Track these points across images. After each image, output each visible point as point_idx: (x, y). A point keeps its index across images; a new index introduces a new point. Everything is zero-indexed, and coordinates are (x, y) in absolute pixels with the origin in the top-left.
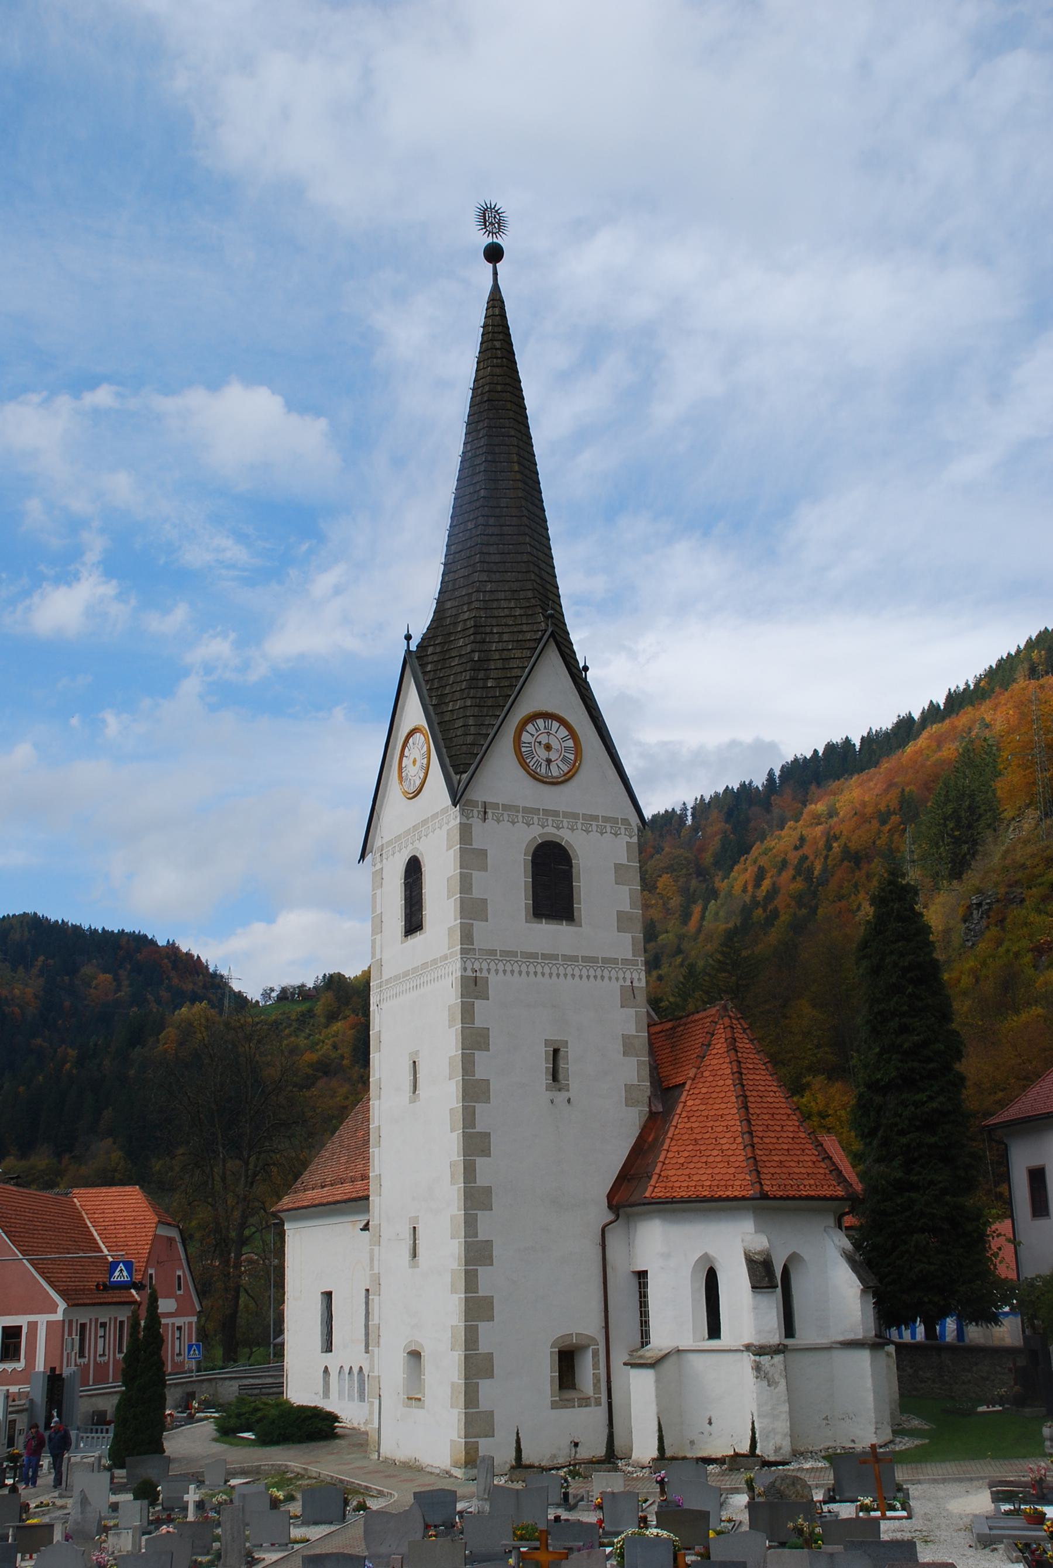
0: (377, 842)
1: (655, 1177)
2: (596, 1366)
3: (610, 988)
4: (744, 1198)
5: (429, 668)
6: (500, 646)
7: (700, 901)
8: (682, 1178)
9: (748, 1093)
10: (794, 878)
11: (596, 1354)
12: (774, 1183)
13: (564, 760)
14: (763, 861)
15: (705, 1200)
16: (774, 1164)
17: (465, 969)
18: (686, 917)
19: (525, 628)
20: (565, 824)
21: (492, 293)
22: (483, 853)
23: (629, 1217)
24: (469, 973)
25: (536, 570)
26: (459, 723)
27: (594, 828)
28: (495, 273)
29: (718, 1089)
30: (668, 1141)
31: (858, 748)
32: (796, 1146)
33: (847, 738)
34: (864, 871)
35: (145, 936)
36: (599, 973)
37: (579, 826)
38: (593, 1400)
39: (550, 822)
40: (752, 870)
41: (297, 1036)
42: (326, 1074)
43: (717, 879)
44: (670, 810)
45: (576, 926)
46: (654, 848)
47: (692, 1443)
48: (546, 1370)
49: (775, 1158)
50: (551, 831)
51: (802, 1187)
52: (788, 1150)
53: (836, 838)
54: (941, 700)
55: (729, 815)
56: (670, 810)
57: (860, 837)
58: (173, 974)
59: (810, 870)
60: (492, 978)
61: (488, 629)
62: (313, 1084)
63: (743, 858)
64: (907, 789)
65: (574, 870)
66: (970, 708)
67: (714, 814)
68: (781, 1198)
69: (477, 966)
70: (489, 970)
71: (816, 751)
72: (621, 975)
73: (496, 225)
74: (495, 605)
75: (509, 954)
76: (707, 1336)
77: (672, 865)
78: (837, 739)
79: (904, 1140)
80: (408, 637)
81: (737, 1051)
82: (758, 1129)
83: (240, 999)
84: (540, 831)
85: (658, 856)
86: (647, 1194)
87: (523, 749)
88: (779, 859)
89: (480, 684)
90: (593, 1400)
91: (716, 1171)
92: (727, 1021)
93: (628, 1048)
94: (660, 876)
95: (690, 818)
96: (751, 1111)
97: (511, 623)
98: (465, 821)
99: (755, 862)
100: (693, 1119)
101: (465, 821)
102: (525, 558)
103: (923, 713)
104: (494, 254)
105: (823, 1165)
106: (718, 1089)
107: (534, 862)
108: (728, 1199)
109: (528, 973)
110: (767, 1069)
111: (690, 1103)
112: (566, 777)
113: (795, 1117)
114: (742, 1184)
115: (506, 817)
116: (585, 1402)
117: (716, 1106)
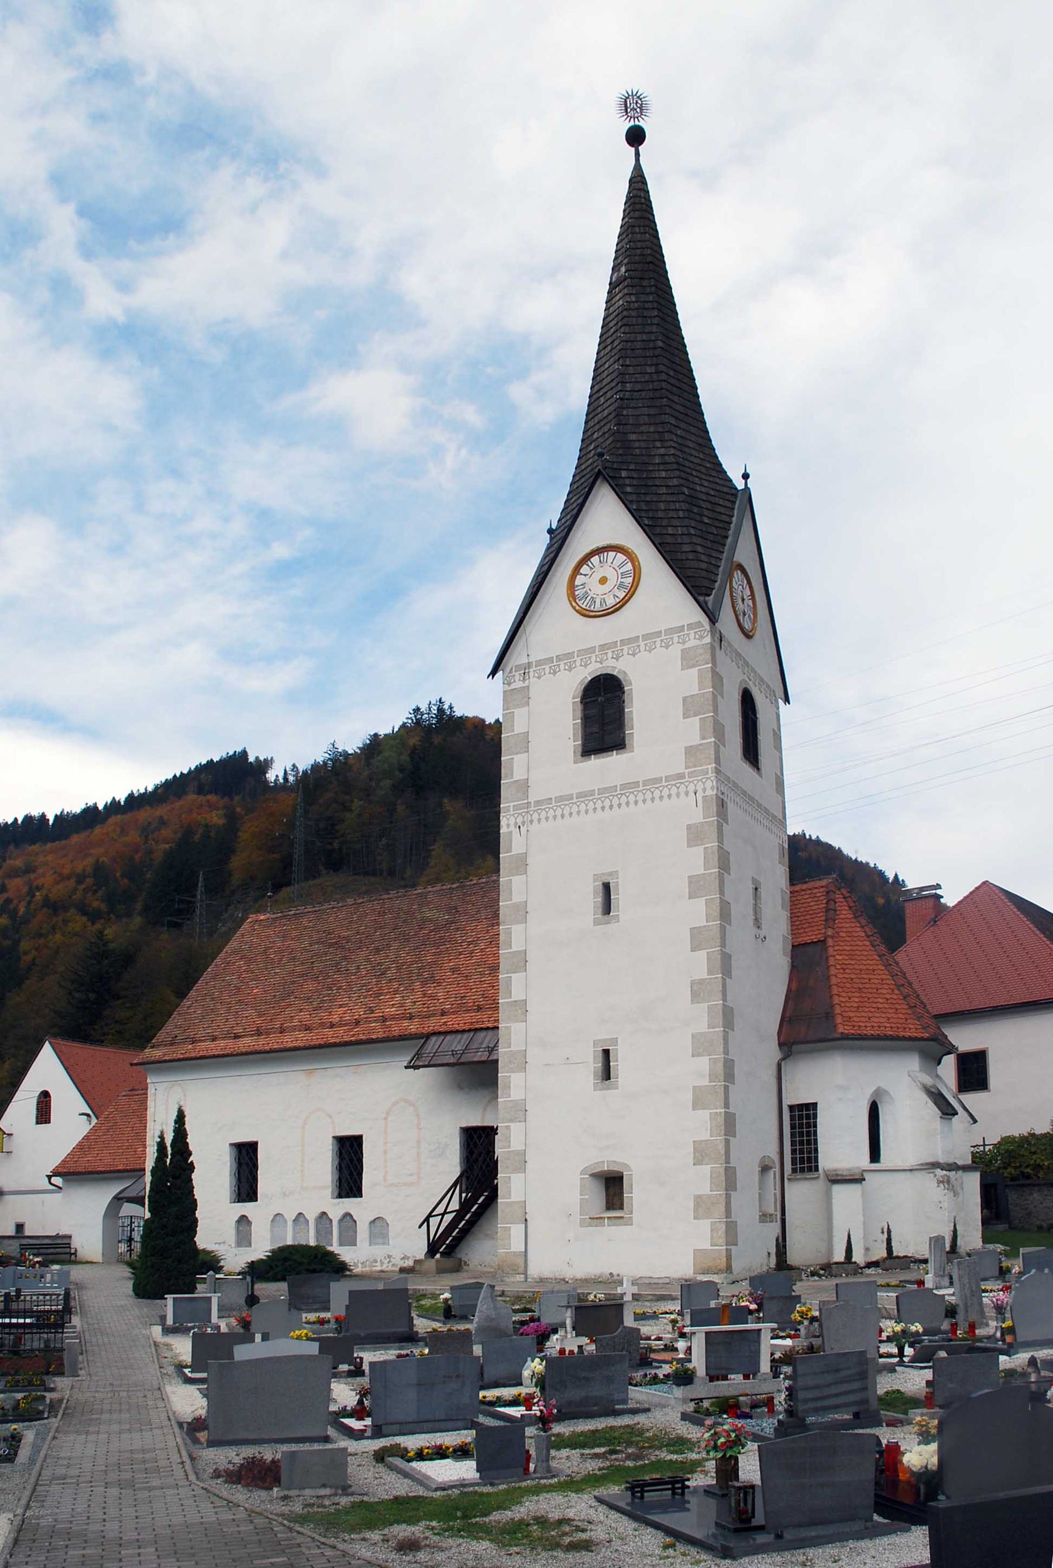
0: (517, 657)
21: (635, 168)
28: (637, 154)
31: (51, 822)
33: (43, 813)
52: (858, 1007)
53: (38, 888)
56: (59, 814)
59: (16, 910)
64: (101, 860)
66: (148, 808)
71: (16, 819)
73: (638, 110)
78: (36, 813)
103: (106, 805)
104: (635, 137)
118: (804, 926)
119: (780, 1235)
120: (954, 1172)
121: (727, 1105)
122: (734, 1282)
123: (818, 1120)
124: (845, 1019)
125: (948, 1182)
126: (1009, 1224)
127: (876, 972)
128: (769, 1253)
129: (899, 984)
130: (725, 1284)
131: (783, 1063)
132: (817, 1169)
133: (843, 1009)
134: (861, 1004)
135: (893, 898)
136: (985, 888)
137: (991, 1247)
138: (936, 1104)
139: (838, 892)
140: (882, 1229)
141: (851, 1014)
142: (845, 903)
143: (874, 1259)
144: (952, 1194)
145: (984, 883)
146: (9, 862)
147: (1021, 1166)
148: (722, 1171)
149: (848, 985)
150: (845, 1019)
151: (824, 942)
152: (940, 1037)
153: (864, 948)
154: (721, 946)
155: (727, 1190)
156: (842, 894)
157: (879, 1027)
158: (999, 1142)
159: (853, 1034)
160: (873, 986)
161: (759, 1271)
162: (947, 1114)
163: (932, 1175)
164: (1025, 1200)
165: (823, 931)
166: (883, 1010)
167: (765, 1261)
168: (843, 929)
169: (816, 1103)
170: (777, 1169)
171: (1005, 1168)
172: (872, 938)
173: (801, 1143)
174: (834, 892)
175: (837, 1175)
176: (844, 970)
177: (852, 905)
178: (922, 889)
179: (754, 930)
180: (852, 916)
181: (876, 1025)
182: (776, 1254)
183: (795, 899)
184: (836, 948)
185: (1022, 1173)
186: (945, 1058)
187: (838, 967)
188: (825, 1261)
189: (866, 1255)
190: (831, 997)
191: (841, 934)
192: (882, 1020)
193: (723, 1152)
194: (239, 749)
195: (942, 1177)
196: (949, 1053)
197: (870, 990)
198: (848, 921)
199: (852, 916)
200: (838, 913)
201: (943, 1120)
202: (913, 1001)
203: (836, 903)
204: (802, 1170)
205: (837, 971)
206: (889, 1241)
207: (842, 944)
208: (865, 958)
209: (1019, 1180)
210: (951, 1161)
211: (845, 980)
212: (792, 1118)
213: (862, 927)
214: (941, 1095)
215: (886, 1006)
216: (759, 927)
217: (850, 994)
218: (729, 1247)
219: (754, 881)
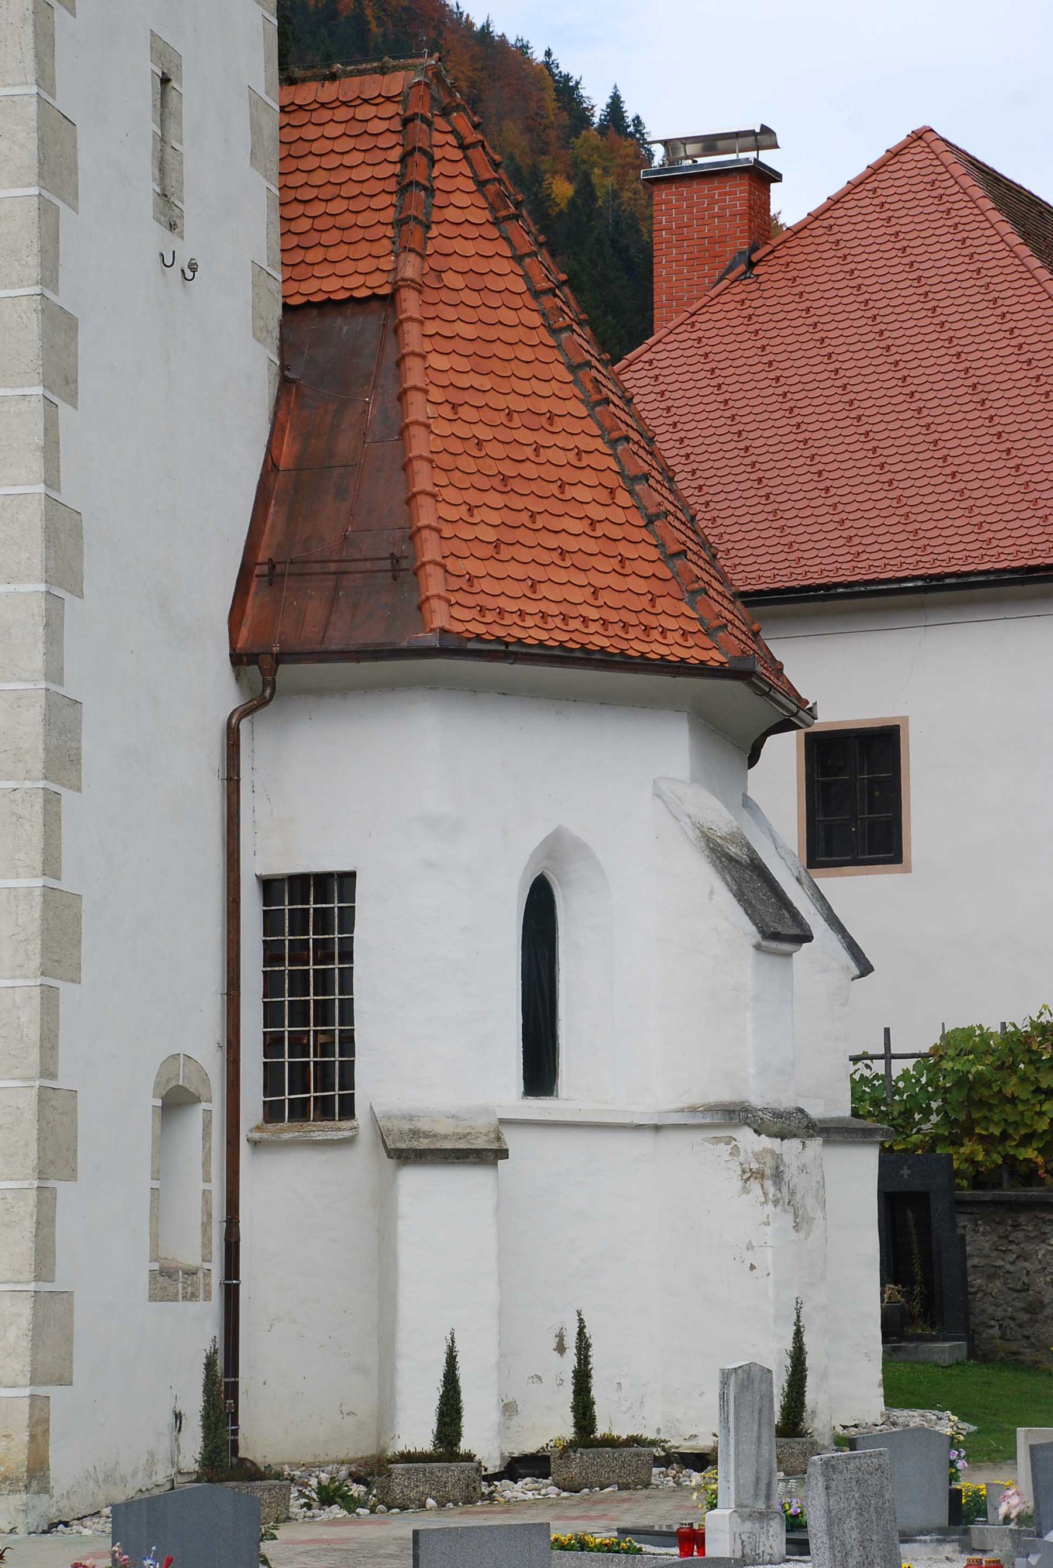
52: (497, 545)
118: (326, 239)
119: (220, 1345)
120: (794, 1144)
121: (51, 865)
122: (52, 1527)
123: (356, 935)
124: (456, 583)
125: (778, 1176)
126: (970, 1341)
127: (559, 424)
128: (178, 1417)
129: (631, 471)
130: (22, 1531)
131: (244, 725)
132: (348, 1110)
133: (448, 548)
134: (509, 536)
135: (603, 183)
136: (918, 153)
137: (913, 1418)
138: (741, 896)
139: (440, 123)
140: (561, 1337)
141: (475, 567)
142: (464, 168)
143: (531, 1446)
144: (789, 1219)
145: (921, 136)
147: (1005, 1136)
148: (28, 1102)
149: (467, 464)
150: (456, 583)
151: (390, 300)
152: (759, 669)
153: (520, 333)
154: (42, 282)
155: (42, 1175)
156: (454, 132)
157: (565, 618)
158: (936, 1048)
159: (478, 637)
160: (553, 473)
161: (141, 1482)
162: (776, 937)
163: (724, 1149)
164: (1023, 1256)
165: (387, 264)
166: (580, 560)
167: (164, 1447)
168: (455, 262)
169: (352, 875)
170: (216, 1104)
171: (955, 1141)
172: (548, 302)
173: (299, 1014)
174: (429, 123)
175: (415, 1133)
176: (454, 407)
177: (487, 173)
178: (710, 143)
179: (155, 236)
180: (487, 215)
181: (553, 609)
182: (206, 1417)
183: (295, 134)
184: (431, 328)
185: (1010, 1161)
186: (772, 741)
187: (436, 395)
188: (363, 1448)
189: (504, 1428)
190: (410, 500)
191: (449, 279)
192: (577, 596)
193: (33, 1033)
195: (757, 1156)
196: (784, 726)
197: (537, 487)
198: (474, 232)
199: (487, 215)
200: (439, 199)
201: (762, 957)
202: (675, 536)
203: (433, 162)
204: (299, 1111)
205: (430, 410)
206: (582, 1378)
207: (450, 314)
208: (525, 371)
209: (998, 1185)
210: (787, 1102)
211: (457, 447)
212: (271, 922)
213: (518, 259)
214: (758, 869)
215: (591, 546)
216: (172, 227)
217: (473, 498)
218: (42, 1391)
219: (160, 49)
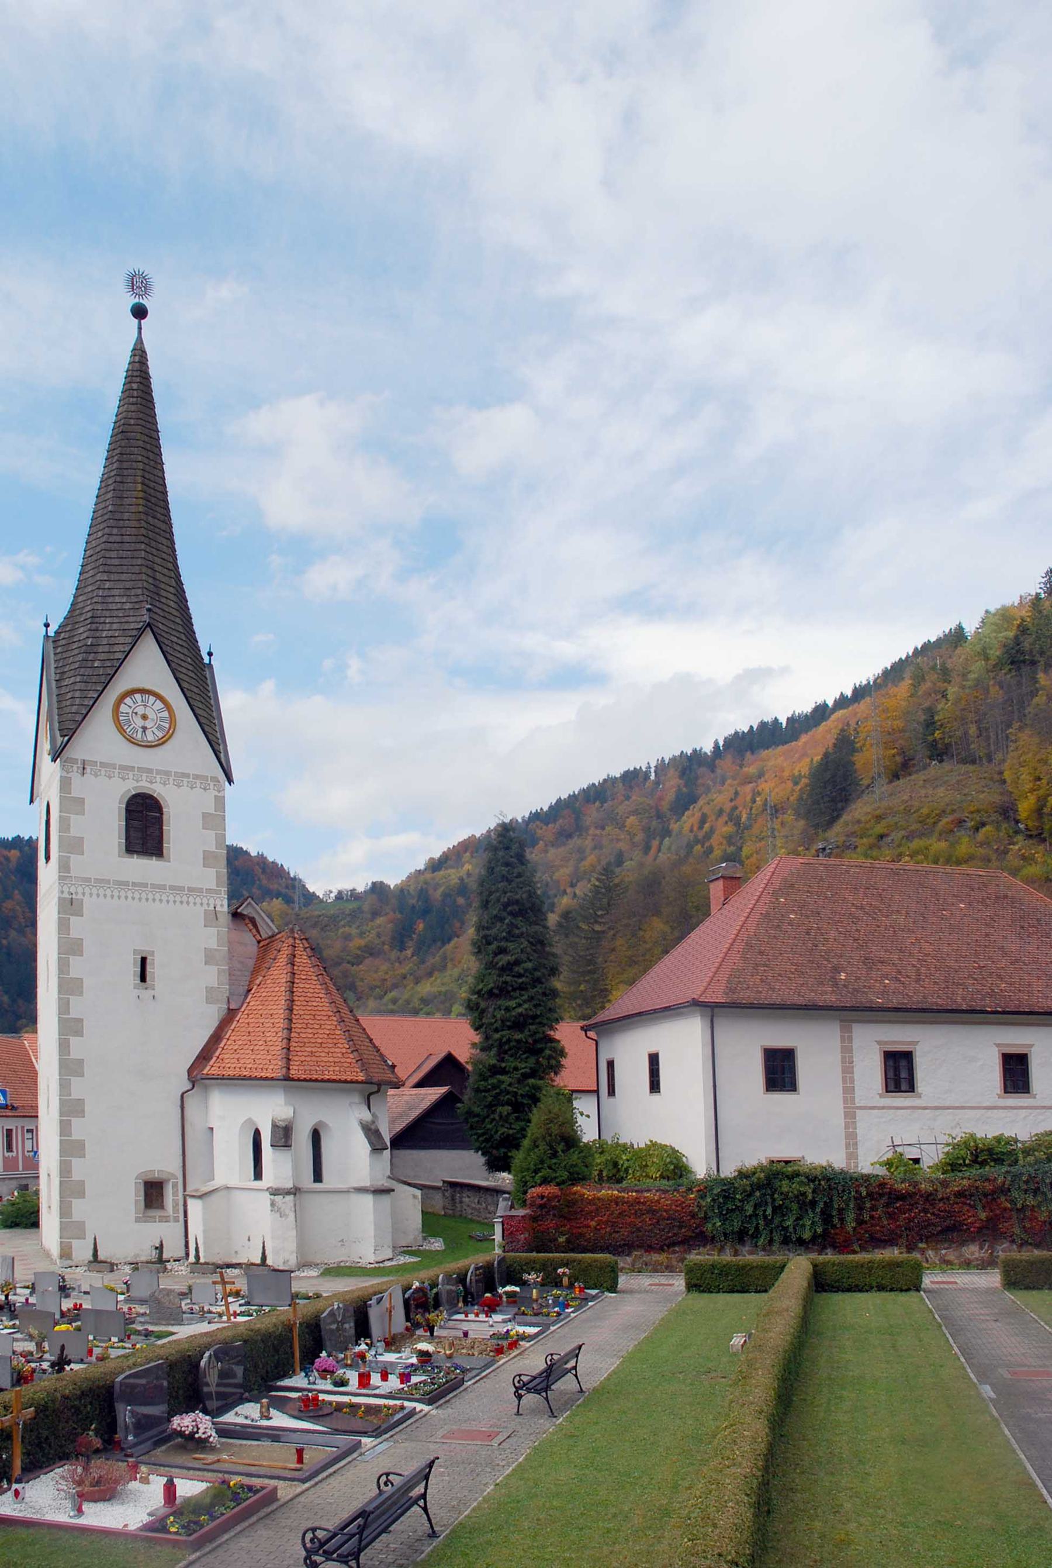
1: (214, 1059)
2: (175, 1194)
3: (195, 912)
4: (272, 1079)
5: (59, 650)
6: (110, 633)
7: (658, 838)
8: (232, 1061)
9: (296, 998)
10: (726, 823)
11: (175, 1185)
12: (302, 1068)
13: (159, 728)
14: (706, 810)
15: (245, 1078)
16: (305, 1054)
17: (62, 892)
18: (647, 849)
19: (131, 619)
20: (158, 780)
22: (82, 801)
23: (206, 1088)
24: (66, 895)
25: (149, 572)
26: (69, 695)
27: (185, 783)
28: (140, 328)
29: (274, 994)
30: (230, 1031)
31: (784, 725)
32: (330, 1041)
34: (779, 820)
35: (242, 848)
36: (185, 898)
37: (171, 781)
38: (172, 1218)
39: (144, 778)
40: (698, 815)
41: (350, 926)
42: (371, 954)
43: (672, 821)
44: (638, 768)
45: (165, 861)
46: (624, 796)
47: (236, 1252)
48: (132, 1196)
49: (307, 1049)
50: (144, 786)
51: (326, 1072)
52: (321, 1043)
53: (759, 794)
54: (849, 693)
55: (683, 773)
57: (777, 793)
58: (262, 877)
59: (739, 818)
60: (87, 900)
61: (102, 620)
62: (361, 963)
63: (692, 807)
65: (165, 817)
67: (672, 772)
68: (305, 1080)
69: (73, 890)
70: (84, 894)
71: (751, 727)
72: (205, 901)
74: (111, 600)
75: (102, 882)
76: (253, 1178)
77: (637, 809)
78: (768, 718)
79: (497, 1036)
80: (47, 625)
81: (294, 965)
82: (297, 1025)
83: (310, 898)
84: (135, 784)
85: (627, 802)
86: (205, 1072)
87: (121, 718)
88: (718, 808)
89: (89, 664)
90: (172, 1218)
91: (258, 1057)
92: (291, 941)
93: (209, 958)
94: (628, 817)
95: (653, 774)
96: (295, 1012)
97: (121, 615)
98: (65, 774)
99: (700, 809)
100: (251, 1016)
101: (65, 774)
102: (139, 562)
103: (835, 701)
104: (140, 312)
105: (351, 1056)
106: (274, 994)
107: (128, 811)
108: (262, 1079)
109: (119, 897)
110: (318, 980)
111: (251, 1004)
112: (160, 742)
113: (335, 1019)
114: (275, 1068)
115: (103, 773)
116: (165, 1219)
117: (270, 1007)
146: (745, 769)
194: (953, 626)
